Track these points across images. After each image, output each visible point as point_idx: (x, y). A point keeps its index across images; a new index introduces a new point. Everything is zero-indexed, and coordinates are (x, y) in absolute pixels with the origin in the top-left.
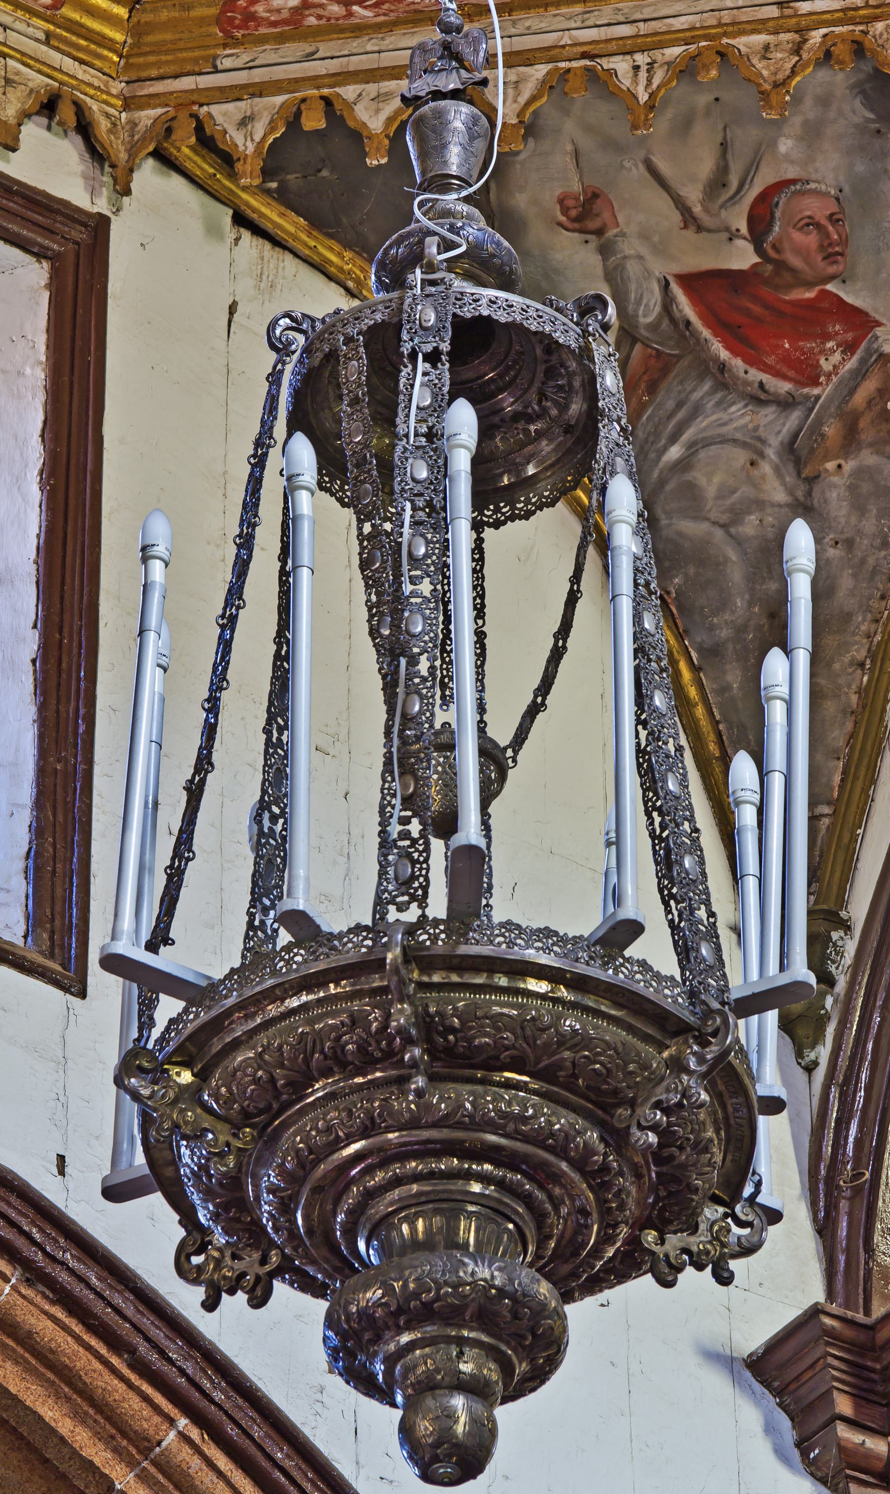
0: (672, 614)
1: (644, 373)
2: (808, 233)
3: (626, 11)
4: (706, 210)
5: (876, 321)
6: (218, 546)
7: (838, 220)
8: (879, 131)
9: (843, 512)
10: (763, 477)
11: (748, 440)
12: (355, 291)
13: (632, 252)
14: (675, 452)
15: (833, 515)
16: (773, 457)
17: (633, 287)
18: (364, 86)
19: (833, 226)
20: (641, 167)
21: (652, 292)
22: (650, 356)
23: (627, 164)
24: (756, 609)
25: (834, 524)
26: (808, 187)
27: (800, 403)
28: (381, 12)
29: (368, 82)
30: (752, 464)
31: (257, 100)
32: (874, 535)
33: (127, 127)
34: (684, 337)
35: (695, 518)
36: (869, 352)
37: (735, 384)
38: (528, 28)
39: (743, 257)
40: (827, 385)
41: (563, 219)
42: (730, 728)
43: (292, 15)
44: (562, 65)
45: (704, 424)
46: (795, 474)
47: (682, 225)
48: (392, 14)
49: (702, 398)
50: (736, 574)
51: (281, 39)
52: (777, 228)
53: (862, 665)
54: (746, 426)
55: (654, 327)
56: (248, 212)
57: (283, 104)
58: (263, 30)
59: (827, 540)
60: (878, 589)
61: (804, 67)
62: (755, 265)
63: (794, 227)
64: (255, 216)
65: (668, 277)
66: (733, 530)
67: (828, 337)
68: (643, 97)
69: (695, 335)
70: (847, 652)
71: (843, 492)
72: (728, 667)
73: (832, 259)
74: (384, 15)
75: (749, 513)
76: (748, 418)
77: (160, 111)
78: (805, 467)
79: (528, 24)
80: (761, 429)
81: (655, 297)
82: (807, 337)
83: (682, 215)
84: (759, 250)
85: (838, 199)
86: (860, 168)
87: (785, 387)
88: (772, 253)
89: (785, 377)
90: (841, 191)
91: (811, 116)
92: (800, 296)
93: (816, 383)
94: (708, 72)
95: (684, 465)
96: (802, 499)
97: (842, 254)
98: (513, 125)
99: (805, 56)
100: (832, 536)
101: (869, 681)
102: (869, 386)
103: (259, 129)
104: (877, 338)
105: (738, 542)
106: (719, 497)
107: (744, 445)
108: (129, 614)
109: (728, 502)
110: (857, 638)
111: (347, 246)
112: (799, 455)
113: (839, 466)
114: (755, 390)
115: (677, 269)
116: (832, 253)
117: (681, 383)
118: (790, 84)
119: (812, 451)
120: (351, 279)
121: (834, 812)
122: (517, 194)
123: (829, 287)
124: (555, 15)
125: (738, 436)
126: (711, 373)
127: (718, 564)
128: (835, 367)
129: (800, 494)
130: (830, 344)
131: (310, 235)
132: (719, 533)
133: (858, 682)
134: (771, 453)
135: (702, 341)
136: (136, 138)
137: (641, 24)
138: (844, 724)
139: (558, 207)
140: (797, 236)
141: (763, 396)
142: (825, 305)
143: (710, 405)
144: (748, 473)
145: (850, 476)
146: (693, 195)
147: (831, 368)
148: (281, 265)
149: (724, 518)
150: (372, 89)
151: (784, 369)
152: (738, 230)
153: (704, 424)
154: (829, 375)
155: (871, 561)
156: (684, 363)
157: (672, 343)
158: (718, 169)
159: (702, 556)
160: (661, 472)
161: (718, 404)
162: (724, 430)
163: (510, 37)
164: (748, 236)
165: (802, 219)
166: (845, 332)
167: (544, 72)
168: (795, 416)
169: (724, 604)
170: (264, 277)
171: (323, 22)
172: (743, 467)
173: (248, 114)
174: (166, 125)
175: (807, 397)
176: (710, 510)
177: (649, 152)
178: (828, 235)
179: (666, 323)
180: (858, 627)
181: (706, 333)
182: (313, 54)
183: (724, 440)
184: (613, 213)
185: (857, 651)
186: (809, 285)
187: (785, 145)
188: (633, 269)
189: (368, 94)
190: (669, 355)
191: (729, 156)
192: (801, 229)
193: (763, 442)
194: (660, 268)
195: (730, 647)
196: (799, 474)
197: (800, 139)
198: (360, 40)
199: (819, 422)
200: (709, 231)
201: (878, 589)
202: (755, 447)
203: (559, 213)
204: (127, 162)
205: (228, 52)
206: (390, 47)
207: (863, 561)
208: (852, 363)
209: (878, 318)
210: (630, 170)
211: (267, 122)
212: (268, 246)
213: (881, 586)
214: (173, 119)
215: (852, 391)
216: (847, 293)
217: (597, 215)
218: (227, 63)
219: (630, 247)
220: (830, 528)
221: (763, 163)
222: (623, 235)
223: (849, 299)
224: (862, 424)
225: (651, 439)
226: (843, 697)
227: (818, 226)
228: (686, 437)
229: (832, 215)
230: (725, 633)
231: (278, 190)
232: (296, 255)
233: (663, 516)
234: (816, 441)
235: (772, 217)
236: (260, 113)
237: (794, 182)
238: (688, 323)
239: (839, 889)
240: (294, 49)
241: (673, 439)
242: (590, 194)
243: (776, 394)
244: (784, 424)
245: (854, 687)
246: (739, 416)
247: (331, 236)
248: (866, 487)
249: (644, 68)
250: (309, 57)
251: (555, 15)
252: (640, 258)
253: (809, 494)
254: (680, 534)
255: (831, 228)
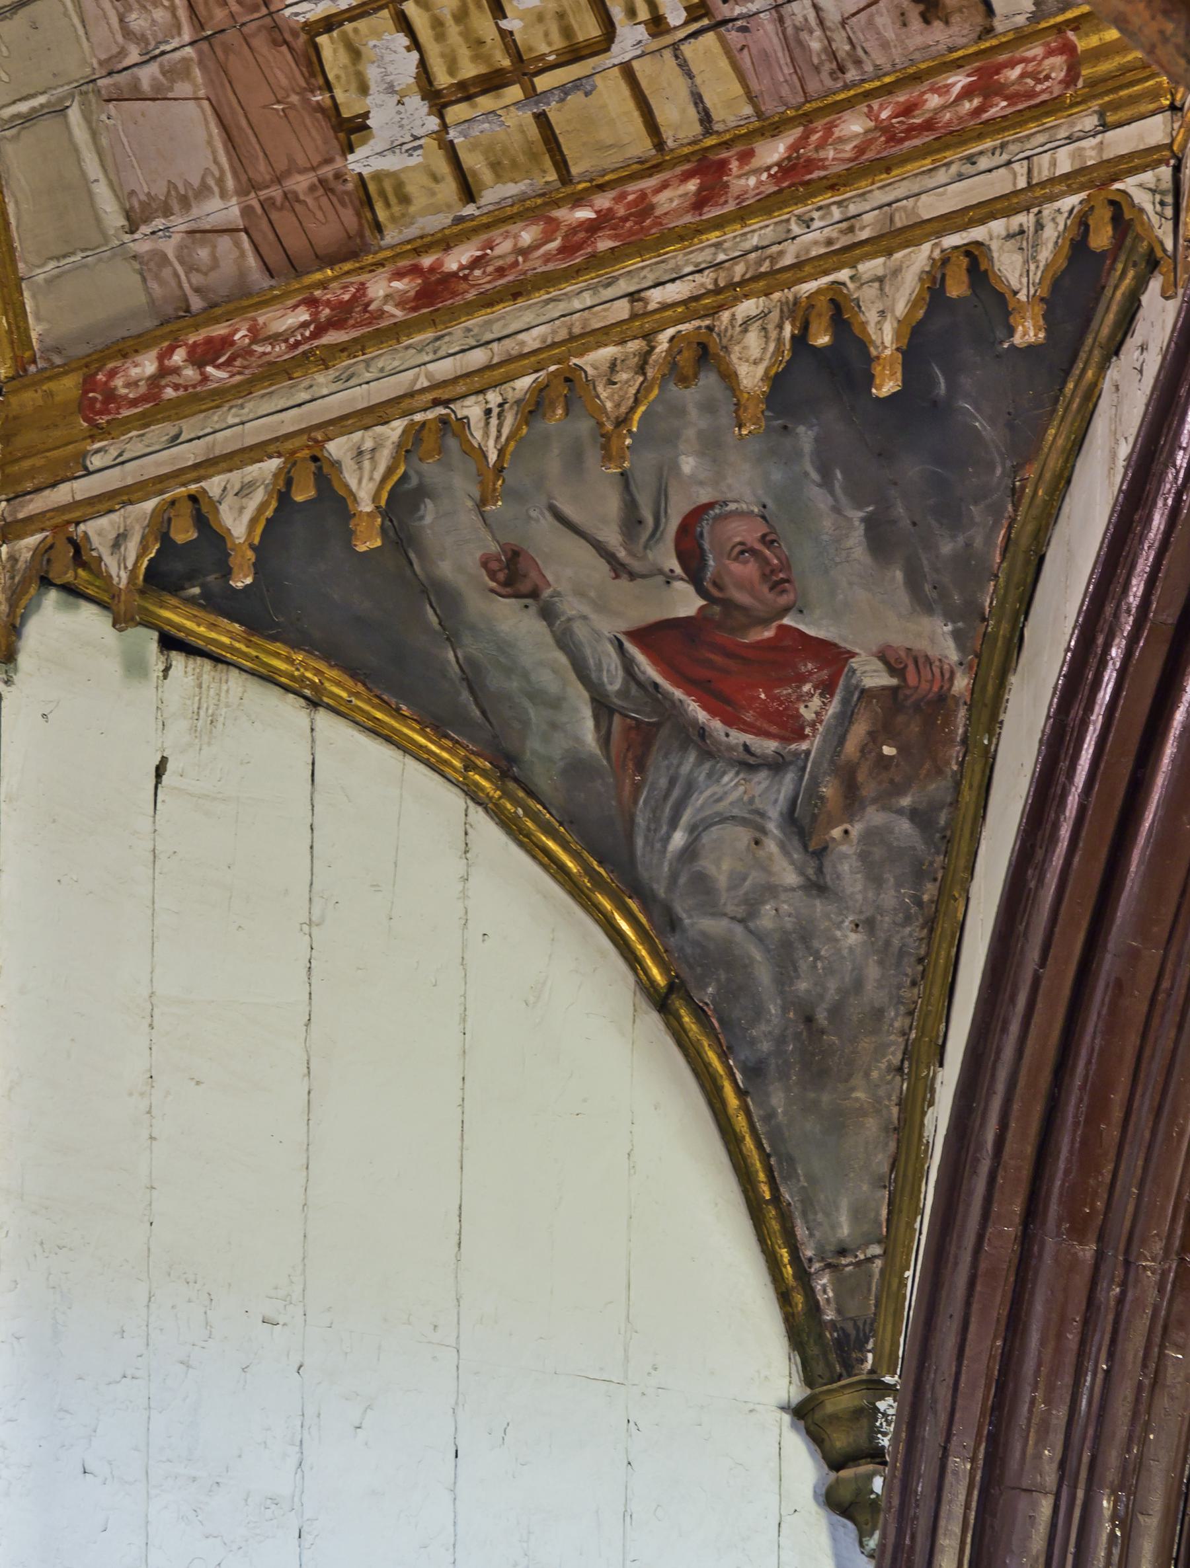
0: (714, 1028)
1: (628, 750)
2: (746, 562)
3: (476, 330)
4: (631, 553)
5: (849, 652)
6: (142, 1094)
7: (773, 541)
8: (785, 427)
9: (859, 887)
10: (770, 857)
11: (747, 816)
12: (315, 699)
13: (574, 612)
14: (679, 839)
15: (849, 890)
16: (776, 832)
17: (588, 652)
18: (229, 475)
19: (768, 549)
20: (547, 514)
21: (609, 655)
22: (630, 728)
23: (534, 514)
24: (791, 1015)
25: (850, 903)
26: (728, 508)
27: (791, 763)
28: (235, 370)
29: (231, 471)
30: (757, 843)
31: (130, 508)
32: (895, 909)
33: (8, 566)
34: (657, 700)
35: (713, 915)
36: (849, 691)
37: (719, 750)
38: (382, 370)
39: (686, 603)
40: (814, 736)
41: (493, 584)
42: (780, 1162)
43: (149, 389)
44: (418, 417)
45: (700, 802)
46: (801, 849)
47: (613, 575)
48: (247, 372)
49: (691, 771)
50: (764, 975)
51: (145, 421)
52: (711, 563)
53: (900, 1069)
54: (741, 799)
55: (624, 693)
56: (173, 631)
57: (154, 510)
58: (125, 413)
59: (846, 924)
60: (907, 975)
61: (649, 390)
62: (702, 608)
63: (729, 557)
64: (182, 635)
65: (619, 636)
66: (751, 925)
67: (802, 679)
68: (493, 457)
69: (667, 696)
70: (884, 1056)
71: (856, 864)
72: (771, 1088)
73: (778, 589)
74: (240, 373)
75: (763, 903)
76: (742, 788)
77: (38, 537)
78: (810, 839)
79: (380, 365)
80: (757, 800)
81: (613, 660)
82: (783, 682)
83: (609, 563)
84: (701, 591)
85: (764, 517)
86: (777, 476)
87: (770, 746)
88: (715, 592)
89: (768, 735)
90: (764, 506)
91: (703, 424)
92: (759, 638)
93: (803, 737)
94: (554, 412)
95: (690, 853)
96: (813, 878)
97: (787, 581)
98: (369, 514)
99: (650, 374)
100: (850, 919)
101: (908, 1088)
102: (859, 731)
103: (132, 548)
104: (854, 671)
105: (759, 937)
106: (732, 887)
107: (744, 822)
108: (34, 1213)
109: (742, 892)
110: (893, 1037)
111: (295, 646)
112: (803, 827)
113: (846, 832)
114: (740, 754)
115: (624, 626)
116: (778, 578)
117: (666, 757)
118: (631, 419)
119: (814, 817)
120: (306, 687)
121: (885, 1252)
122: (440, 563)
123: (786, 621)
124: (407, 348)
125: (736, 812)
126: (693, 741)
127: (745, 966)
128: (817, 713)
129: (810, 872)
130: (807, 688)
131: (249, 643)
132: (739, 929)
133: (898, 1092)
134: (772, 827)
135: (678, 703)
136: (17, 579)
137: (495, 345)
138: (887, 1144)
139: (484, 572)
140: (736, 567)
141: (751, 760)
142: (788, 642)
143: (702, 778)
144: (754, 855)
145: (859, 841)
146: (612, 537)
147: (814, 715)
148: (224, 687)
149: (740, 911)
150: (236, 478)
151: (766, 726)
152: (672, 571)
153: (700, 802)
154: (813, 725)
155: (896, 942)
156: (665, 732)
157: (648, 709)
158: (626, 505)
159: (722, 959)
160: (671, 864)
161: (709, 776)
162: (720, 807)
163: (367, 383)
164: (684, 576)
165: (734, 547)
166: (820, 669)
167: (399, 431)
168: (789, 777)
169: (759, 1012)
170: (202, 713)
171: (181, 393)
172: (748, 848)
173: (121, 530)
174: (45, 558)
175: (796, 754)
176: (725, 904)
177: (550, 497)
178: (766, 561)
179: (634, 690)
180: (891, 1025)
181: (678, 694)
182: (177, 436)
183: (724, 819)
184: (540, 571)
185: (893, 1054)
186: (765, 622)
187: (688, 464)
188: (581, 632)
189: (232, 487)
190: (649, 724)
191: (633, 488)
192: (736, 559)
193: (762, 815)
194: (609, 626)
195: (773, 1061)
196: (805, 847)
197: (701, 454)
198: (220, 412)
199: (815, 782)
200: (643, 576)
201: (907, 975)
202: (754, 821)
203: (487, 578)
204: (8, 616)
205: (97, 445)
206: (251, 416)
207: (888, 943)
208: (834, 707)
209: (849, 647)
210: (537, 521)
211: (138, 540)
212: (208, 665)
213: (909, 971)
214: (51, 547)
215: (842, 740)
216: (806, 624)
217: (525, 576)
218: (96, 462)
219: (571, 606)
220: (847, 908)
221: (671, 491)
222: (558, 594)
223: (807, 631)
224: (861, 777)
225: (653, 827)
226: (884, 1112)
227: (753, 552)
228: (686, 818)
229: (764, 536)
230: (766, 1046)
231: (203, 595)
232: (241, 669)
233: (684, 916)
234: (816, 805)
235: (702, 551)
236: (133, 527)
237: (710, 506)
238: (656, 686)
239: (892, 1345)
240: (159, 432)
241: (673, 824)
242: (510, 553)
243: (764, 756)
244: (779, 791)
245: (894, 1098)
246: (731, 788)
247: (274, 639)
248: (878, 853)
249: (496, 411)
250: (174, 440)
251: (407, 348)
252: (585, 618)
253: (820, 870)
254: (703, 934)
255: (767, 552)
